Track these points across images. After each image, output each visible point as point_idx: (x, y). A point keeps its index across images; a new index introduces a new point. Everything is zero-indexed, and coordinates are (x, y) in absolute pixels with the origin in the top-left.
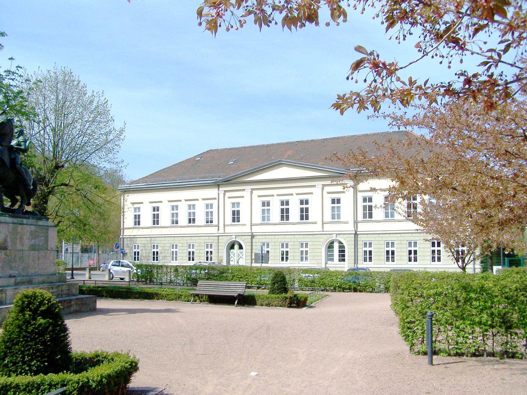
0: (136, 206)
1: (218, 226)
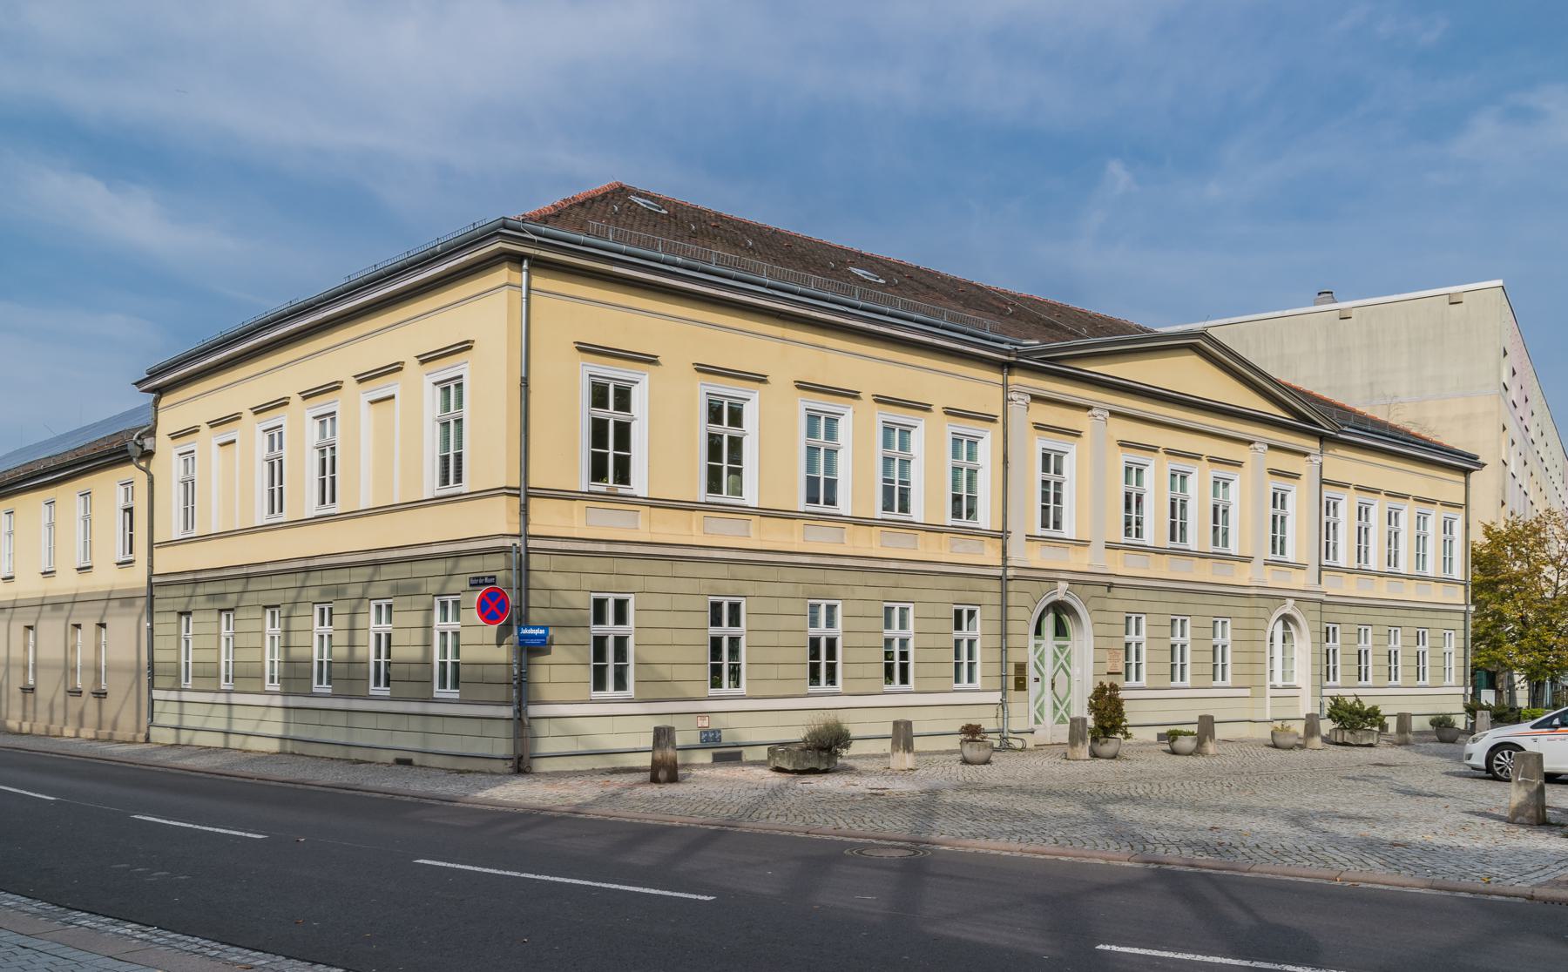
0: (1137, 457)
1: (1003, 535)
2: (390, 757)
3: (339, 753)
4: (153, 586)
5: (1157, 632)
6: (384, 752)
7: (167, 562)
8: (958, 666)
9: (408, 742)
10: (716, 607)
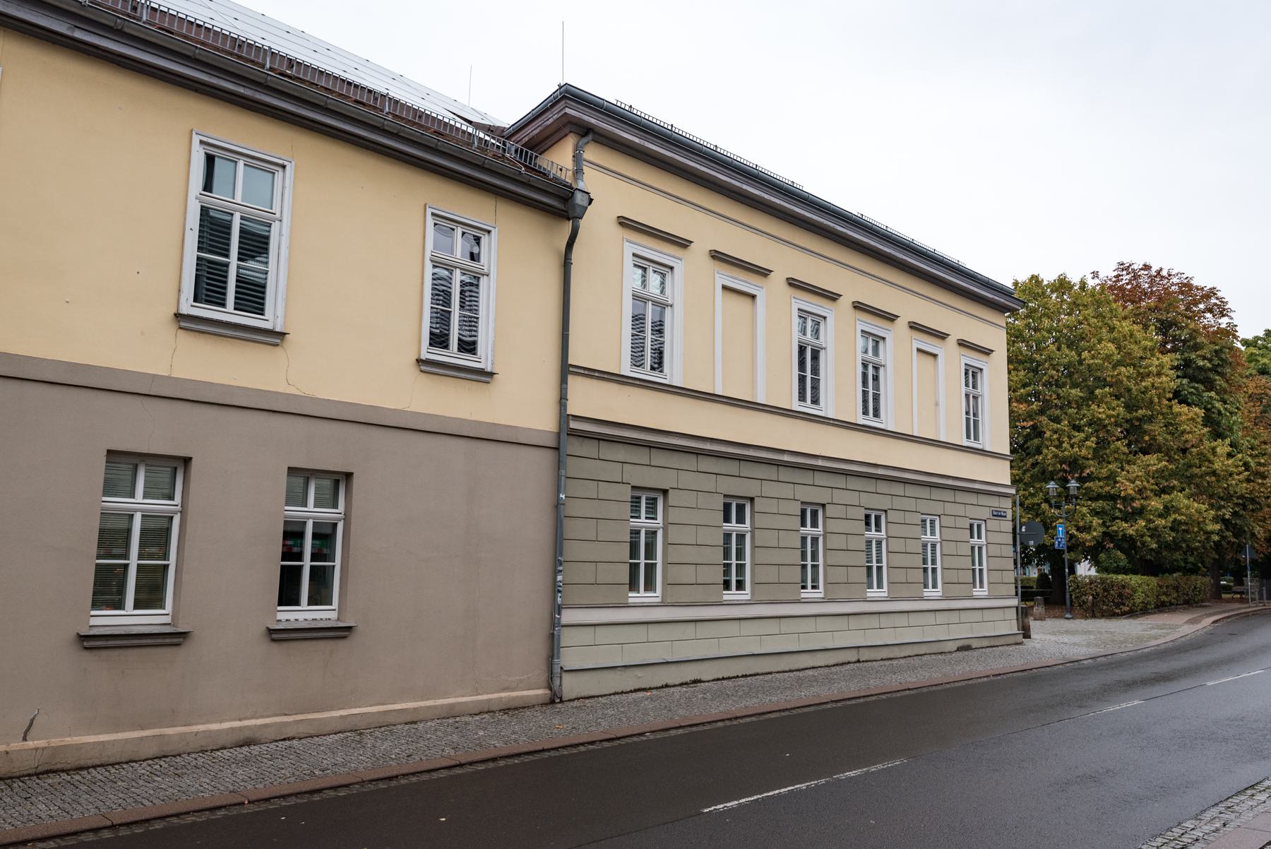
2: (952, 646)
3: (852, 656)
4: (572, 435)
5: (949, 534)
6: (950, 643)
7: (590, 401)
8: (634, 568)
9: (962, 631)
10: (867, 517)
